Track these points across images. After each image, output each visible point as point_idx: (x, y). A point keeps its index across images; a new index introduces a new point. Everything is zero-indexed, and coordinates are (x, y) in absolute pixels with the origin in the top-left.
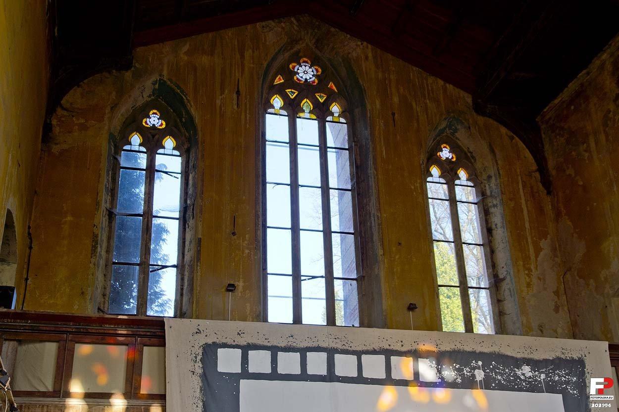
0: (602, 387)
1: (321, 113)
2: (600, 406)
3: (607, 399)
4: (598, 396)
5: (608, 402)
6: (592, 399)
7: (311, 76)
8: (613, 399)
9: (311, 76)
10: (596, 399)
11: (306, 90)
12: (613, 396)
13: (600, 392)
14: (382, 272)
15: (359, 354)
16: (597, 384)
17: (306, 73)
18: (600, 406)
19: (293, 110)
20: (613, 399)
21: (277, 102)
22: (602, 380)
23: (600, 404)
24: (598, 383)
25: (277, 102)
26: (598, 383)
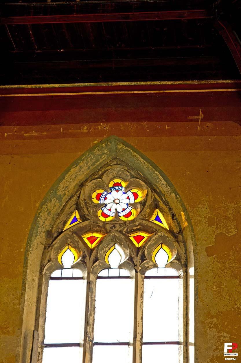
0: (231, 348)
1: (139, 263)
2: (230, 360)
3: (234, 355)
4: (229, 354)
5: (235, 357)
6: (225, 355)
7: (126, 207)
8: (237, 355)
9: (126, 207)
10: (227, 355)
11: (119, 231)
12: (237, 354)
13: (229, 351)
14: (175, 83)
15: (134, 345)
16: (228, 347)
17: (118, 202)
18: (230, 360)
19: (92, 262)
20: (237, 355)
21: (69, 257)
22: (231, 344)
23: (230, 359)
24: (228, 346)
25: (69, 257)
26: (228, 346)
